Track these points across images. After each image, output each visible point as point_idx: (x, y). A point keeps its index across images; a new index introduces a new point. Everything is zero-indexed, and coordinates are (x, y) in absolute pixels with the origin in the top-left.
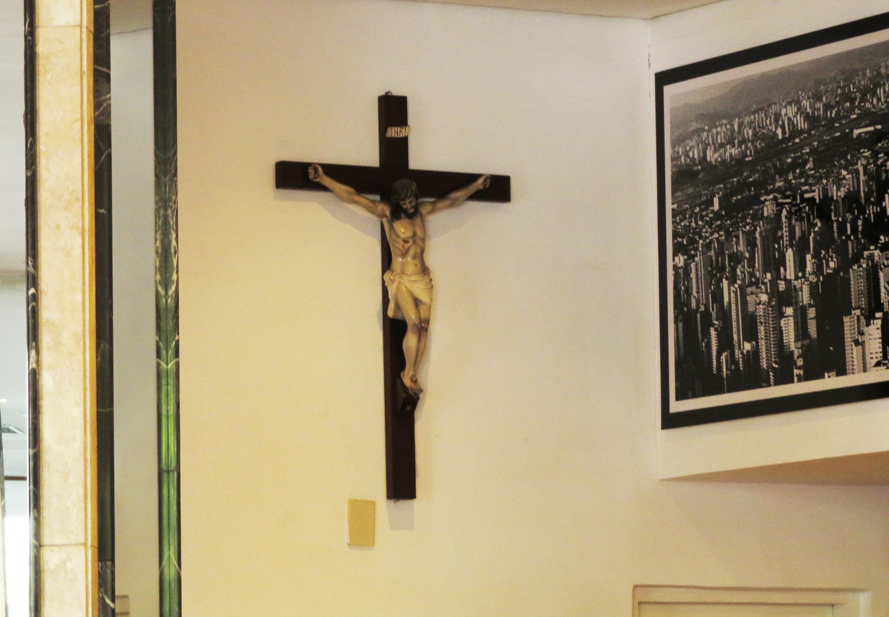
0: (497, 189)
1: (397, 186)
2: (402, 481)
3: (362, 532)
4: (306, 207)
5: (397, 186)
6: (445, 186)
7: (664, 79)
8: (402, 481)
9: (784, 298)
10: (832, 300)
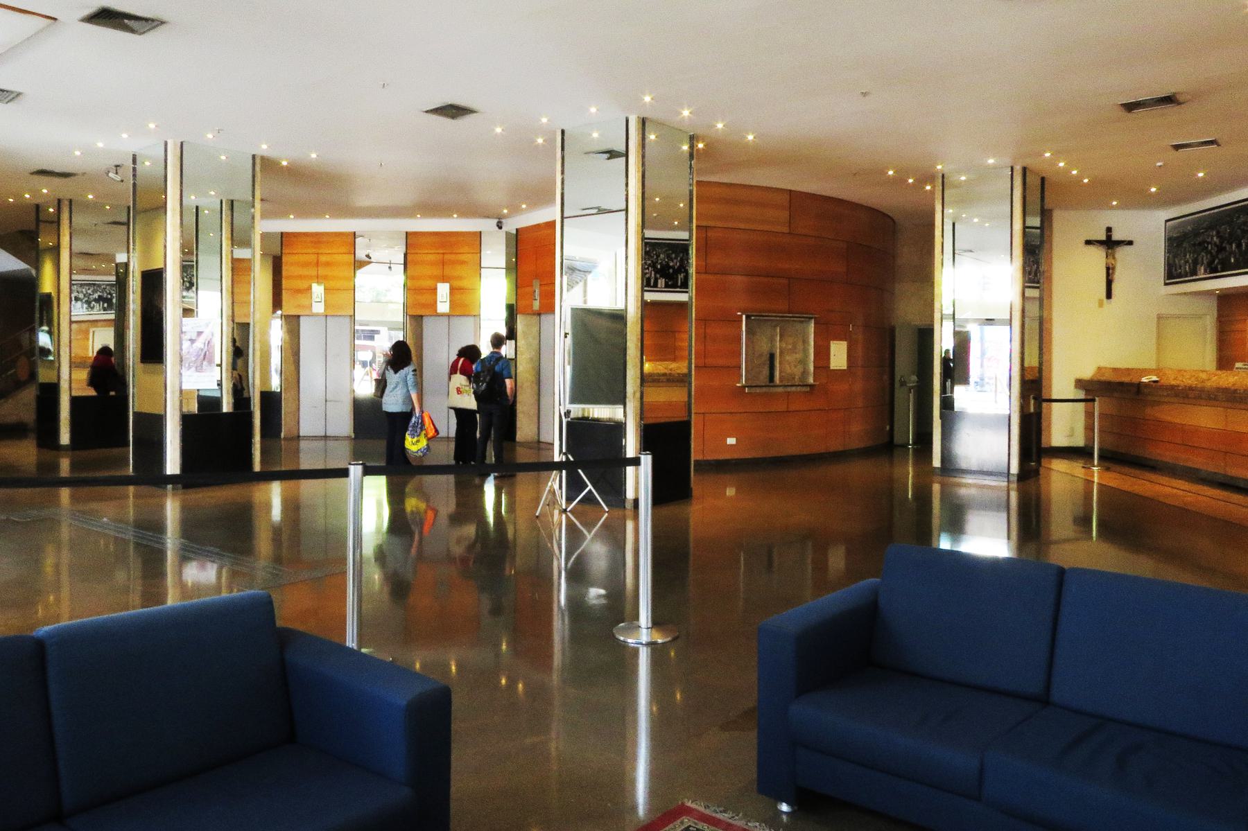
0: (1130, 243)
1: (1110, 243)
2: (1109, 295)
3: (1101, 304)
4: (1092, 248)
5: (1110, 243)
6: (1120, 243)
7: (1167, 221)
8: (1109, 295)
9: (1187, 262)
10: (1195, 262)
